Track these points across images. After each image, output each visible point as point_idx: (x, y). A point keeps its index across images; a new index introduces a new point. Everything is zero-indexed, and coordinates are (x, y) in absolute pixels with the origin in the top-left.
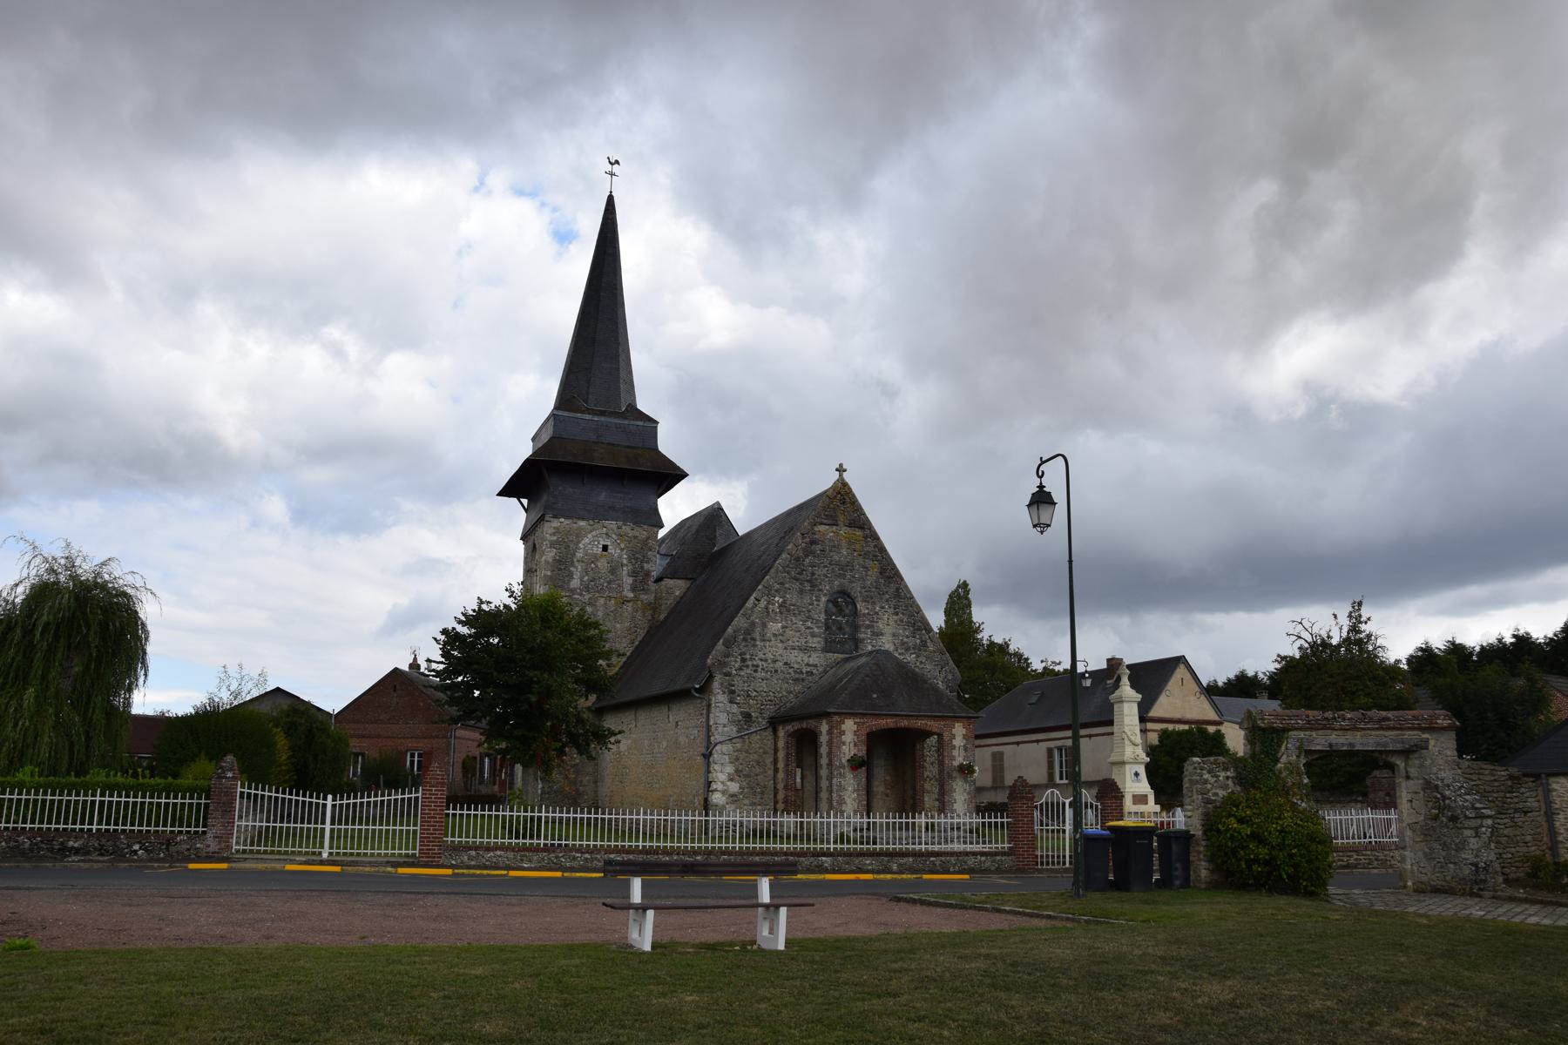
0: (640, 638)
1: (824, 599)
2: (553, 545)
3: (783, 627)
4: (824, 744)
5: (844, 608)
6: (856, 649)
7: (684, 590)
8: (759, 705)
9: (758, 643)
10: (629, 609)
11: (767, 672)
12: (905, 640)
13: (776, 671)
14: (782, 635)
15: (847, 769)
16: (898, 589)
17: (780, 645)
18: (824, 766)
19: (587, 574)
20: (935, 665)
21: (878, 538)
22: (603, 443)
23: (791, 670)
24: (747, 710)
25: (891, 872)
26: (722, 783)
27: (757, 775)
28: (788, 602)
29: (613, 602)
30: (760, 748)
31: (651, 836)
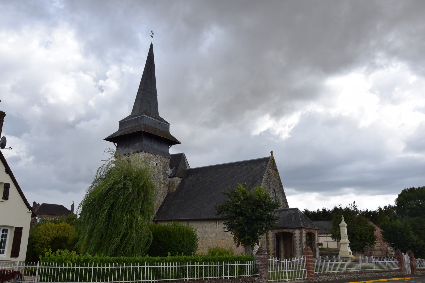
0: (165, 196)
10: (163, 186)
29: (159, 183)
31: (284, 273)
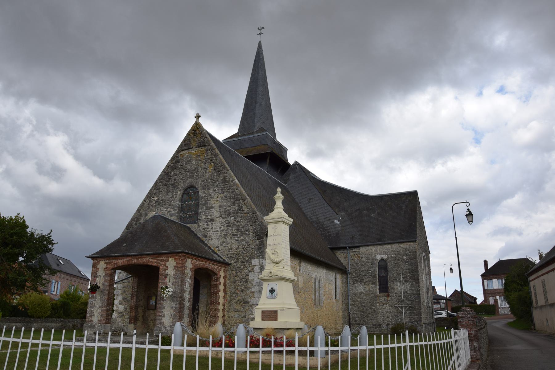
12: (228, 208)
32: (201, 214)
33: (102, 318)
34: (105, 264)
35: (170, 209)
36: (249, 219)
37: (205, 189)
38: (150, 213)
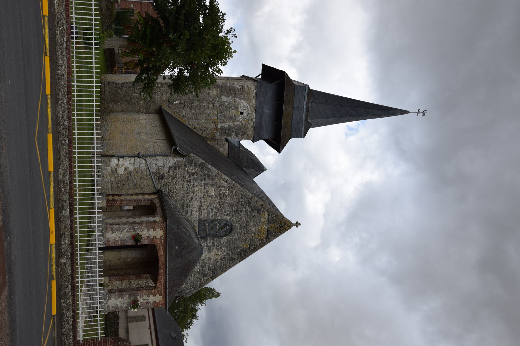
0: (197, 132)
1: (228, 218)
2: (242, 86)
3: (212, 196)
4: (148, 219)
5: (223, 230)
6: (202, 238)
7: (223, 152)
8: (168, 184)
9: (203, 182)
10: (212, 126)
11: (187, 188)
12: (207, 265)
13: (188, 193)
14: (207, 196)
15: (133, 233)
16: (234, 259)
17: (202, 195)
18: (135, 220)
19: (228, 104)
20: (193, 282)
21: (261, 247)
22: (293, 111)
23: (188, 201)
24: (165, 177)
25: (58, 258)
26: (123, 164)
27: (128, 184)
28: (226, 198)
29: (215, 118)
30: (144, 186)
32: (205, 243)
33: (111, 243)
34: (160, 236)
35: (214, 211)
36: (196, 283)
37: (227, 243)
38: (214, 189)
